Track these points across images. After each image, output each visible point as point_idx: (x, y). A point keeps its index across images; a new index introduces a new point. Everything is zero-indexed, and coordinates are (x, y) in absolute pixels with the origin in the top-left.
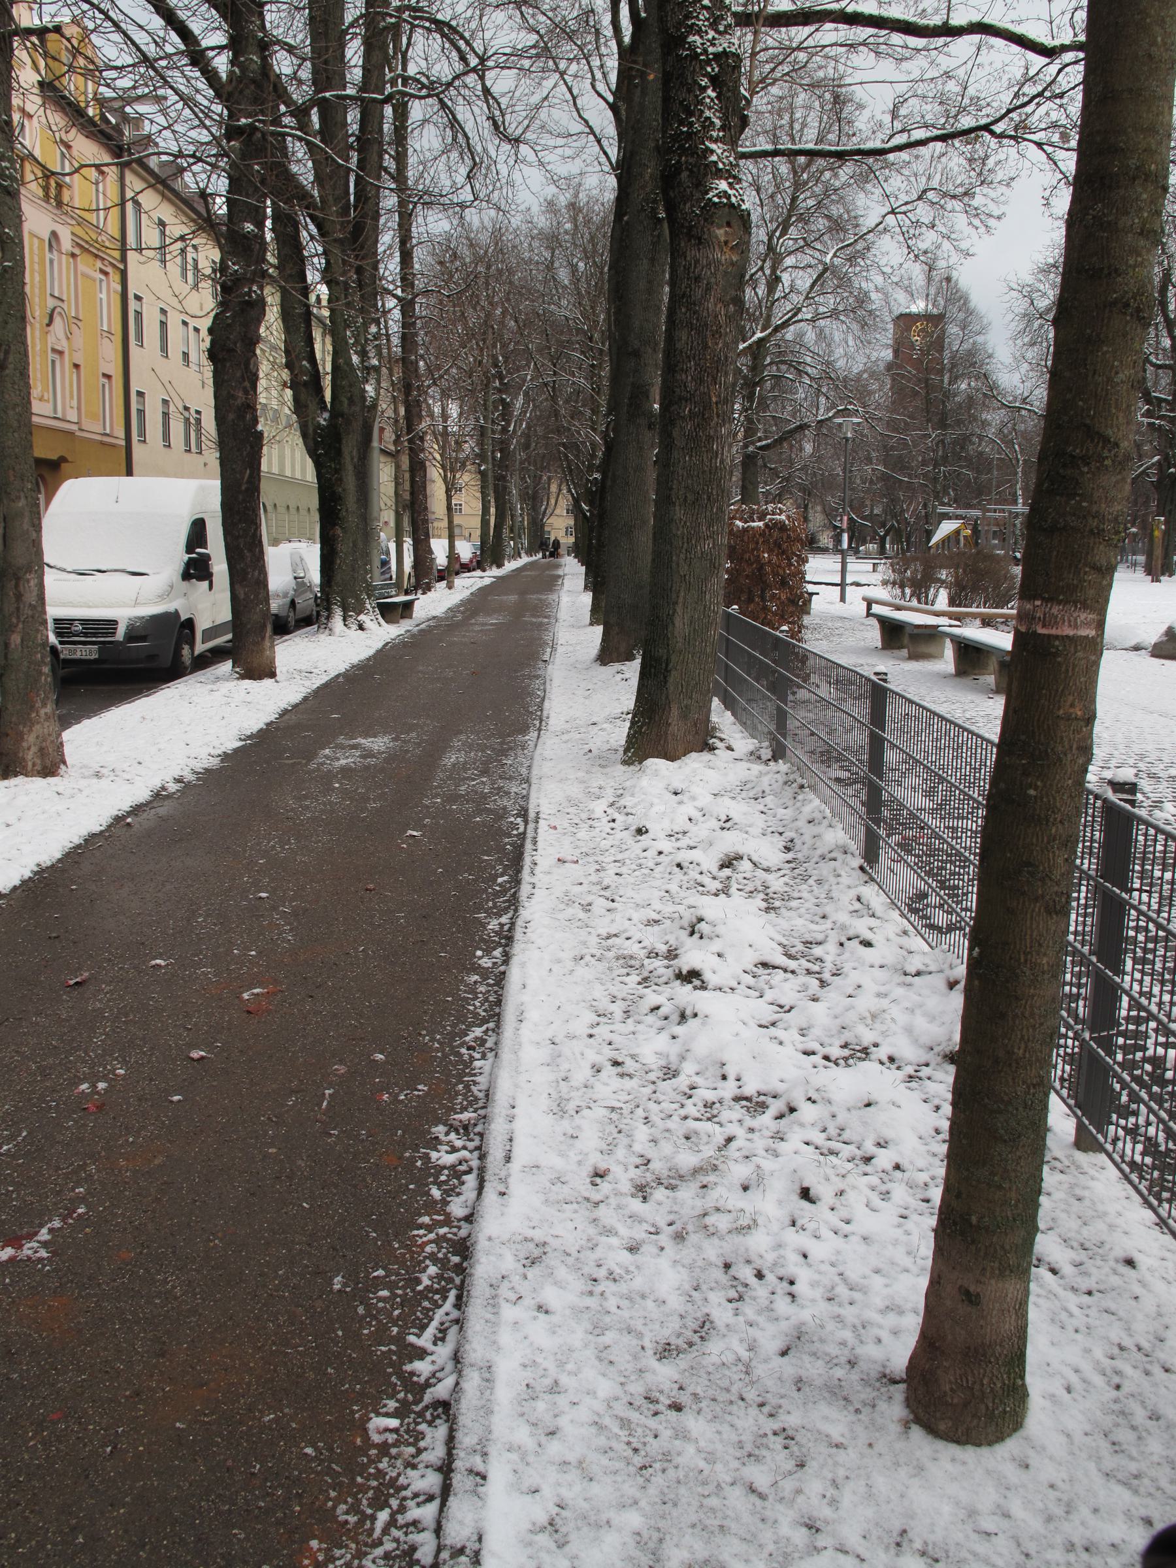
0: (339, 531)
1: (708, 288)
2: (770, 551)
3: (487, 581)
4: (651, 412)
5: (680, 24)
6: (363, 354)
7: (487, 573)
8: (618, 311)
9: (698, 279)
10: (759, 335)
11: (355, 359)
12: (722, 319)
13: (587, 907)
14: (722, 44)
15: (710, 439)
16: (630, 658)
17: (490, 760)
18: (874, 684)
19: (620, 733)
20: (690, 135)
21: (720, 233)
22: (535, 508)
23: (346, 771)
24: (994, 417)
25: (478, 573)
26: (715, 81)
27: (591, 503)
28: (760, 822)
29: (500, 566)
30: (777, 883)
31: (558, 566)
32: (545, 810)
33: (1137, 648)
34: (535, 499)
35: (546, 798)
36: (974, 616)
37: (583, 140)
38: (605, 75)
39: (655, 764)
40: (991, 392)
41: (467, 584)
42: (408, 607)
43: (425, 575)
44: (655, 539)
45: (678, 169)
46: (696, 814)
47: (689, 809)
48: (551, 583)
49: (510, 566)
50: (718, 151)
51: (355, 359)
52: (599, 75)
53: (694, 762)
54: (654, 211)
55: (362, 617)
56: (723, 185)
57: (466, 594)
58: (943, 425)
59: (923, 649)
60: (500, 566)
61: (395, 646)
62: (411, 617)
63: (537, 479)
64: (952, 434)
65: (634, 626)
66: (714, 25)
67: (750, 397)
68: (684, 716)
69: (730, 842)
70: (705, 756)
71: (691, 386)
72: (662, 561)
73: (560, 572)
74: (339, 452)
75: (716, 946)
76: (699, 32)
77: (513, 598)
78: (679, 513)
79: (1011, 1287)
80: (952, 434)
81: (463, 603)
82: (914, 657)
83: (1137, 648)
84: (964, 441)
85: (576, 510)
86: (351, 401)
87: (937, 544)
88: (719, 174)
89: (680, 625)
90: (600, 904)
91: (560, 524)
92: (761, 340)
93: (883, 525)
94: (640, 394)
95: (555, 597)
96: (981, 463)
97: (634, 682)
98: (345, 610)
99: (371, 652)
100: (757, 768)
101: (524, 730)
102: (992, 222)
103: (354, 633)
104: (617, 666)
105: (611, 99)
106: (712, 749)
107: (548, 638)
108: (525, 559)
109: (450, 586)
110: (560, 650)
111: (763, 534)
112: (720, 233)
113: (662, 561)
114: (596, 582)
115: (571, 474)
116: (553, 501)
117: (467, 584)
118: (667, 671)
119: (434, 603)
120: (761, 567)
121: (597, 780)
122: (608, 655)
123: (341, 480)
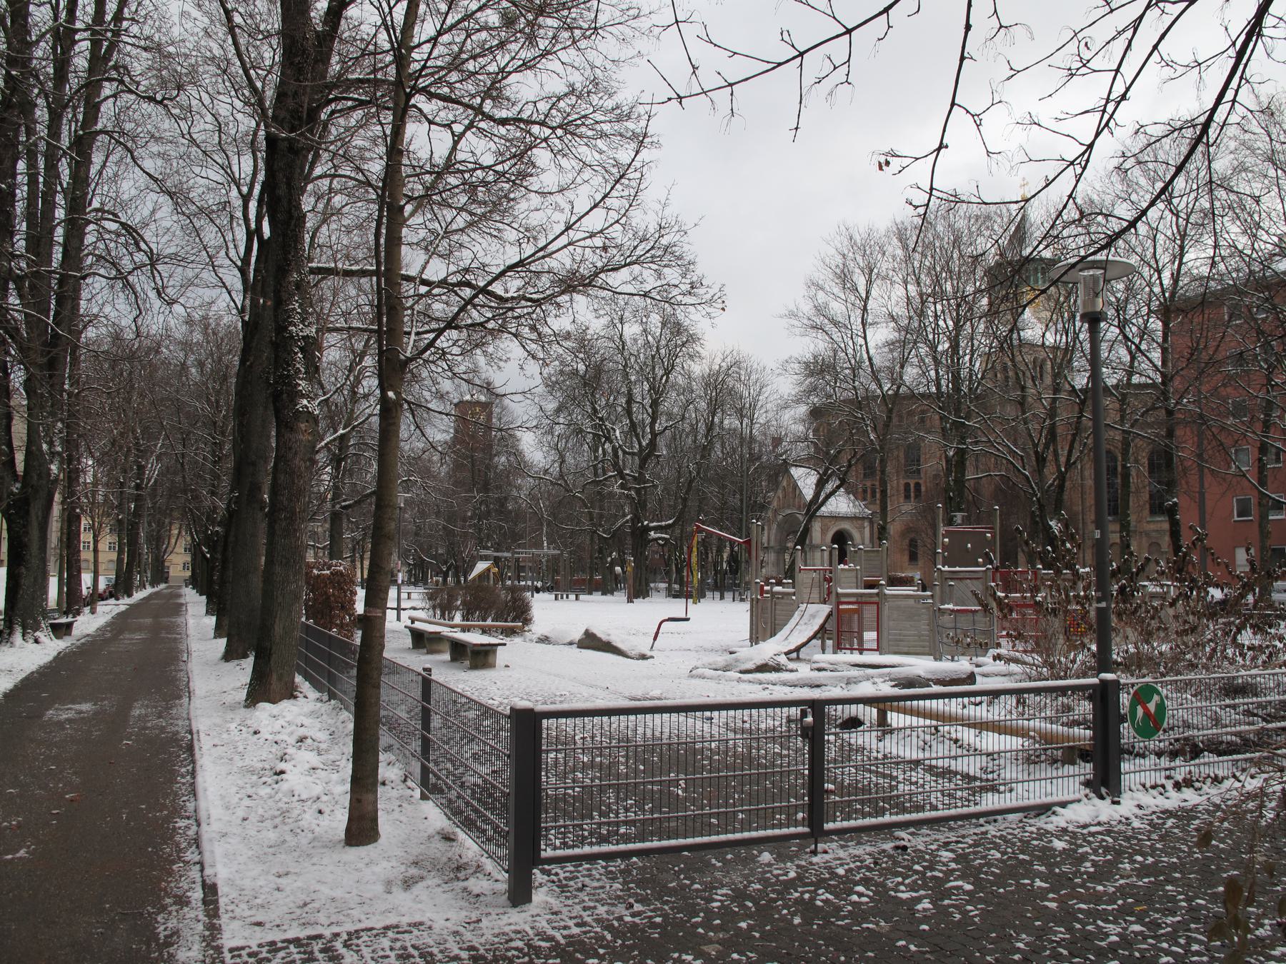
0: (23, 570)
1: (296, 453)
2: (334, 588)
3: (123, 608)
4: (263, 501)
5: (285, 320)
6: (51, 444)
7: (120, 602)
8: (241, 425)
9: (290, 448)
10: (341, 432)
11: (45, 447)
12: (303, 469)
13: (231, 760)
14: (307, 332)
15: (295, 530)
16: (245, 656)
17: (161, 712)
18: (424, 678)
19: (243, 695)
20: (288, 376)
21: (303, 426)
22: (158, 548)
23: (69, 721)
24: (526, 483)
25: (112, 601)
26: (302, 350)
27: (212, 549)
28: (319, 725)
29: (130, 595)
30: (323, 746)
31: (180, 596)
32: (202, 728)
33: (571, 643)
34: (158, 541)
35: (201, 724)
36: (474, 626)
37: (218, 290)
38: (235, 246)
39: (262, 705)
40: (520, 466)
41: (108, 611)
42: (69, 626)
43: (73, 601)
44: (264, 582)
45: (282, 393)
46: (285, 724)
47: (281, 722)
48: (177, 609)
49: (138, 596)
50: (303, 385)
51: (45, 447)
52: (231, 245)
53: (285, 705)
54: (268, 379)
55: (38, 634)
56: (305, 402)
57: (108, 618)
58: (485, 488)
59: (435, 647)
60: (130, 595)
61: (66, 654)
62: (70, 634)
63: (161, 525)
64: (494, 495)
65: (247, 634)
66: (303, 322)
67: (337, 468)
68: (280, 679)
69: (302, 732)
70: (292, 701)
71: (286, 503)
72: (268, 594)
73: (182, 600)
74: (27, 512)
75: (293, 762)
76: (295, 325)
77: (148, 621)
78: (278, 569)
79: (370, 797)
80: (494, 495)
81: (108, 624)
82: (430, 652)
83: (571, 643)
84: (502, 502)
85: (194, 550)
86: (40, 476)
87: (474, 579)
88: (303, 396)
89: (278, 629)
90: (237, 758)
91: (178, 561)
92: (342, 435)
93: (445, 563)
94: (255, 489)
95: (182, 619)
96: (518, 516)
97: (249, 670)
98: (24, 628)
99: (50, 658)
100: (319, 705)
101: (180, 697)
102: (501, 364)
103: (31, 645)
104: (236, 662)
105: (239, 263)
106: (296, 697)
107: (183, 647)
108: (149, 590)
109: (93, 612)
110: (194, 654)
111: (329, 578)
112: (303, 426)
113: (268, 594)
114: (217, 606)
115: (194, 521)
116: (173, 541)
117: (108, 611)
118: (270, 654)
119: (87, 624)
120: (328, 598)
121: (230, 715)
122: (229, 656)
123: (27, 533)
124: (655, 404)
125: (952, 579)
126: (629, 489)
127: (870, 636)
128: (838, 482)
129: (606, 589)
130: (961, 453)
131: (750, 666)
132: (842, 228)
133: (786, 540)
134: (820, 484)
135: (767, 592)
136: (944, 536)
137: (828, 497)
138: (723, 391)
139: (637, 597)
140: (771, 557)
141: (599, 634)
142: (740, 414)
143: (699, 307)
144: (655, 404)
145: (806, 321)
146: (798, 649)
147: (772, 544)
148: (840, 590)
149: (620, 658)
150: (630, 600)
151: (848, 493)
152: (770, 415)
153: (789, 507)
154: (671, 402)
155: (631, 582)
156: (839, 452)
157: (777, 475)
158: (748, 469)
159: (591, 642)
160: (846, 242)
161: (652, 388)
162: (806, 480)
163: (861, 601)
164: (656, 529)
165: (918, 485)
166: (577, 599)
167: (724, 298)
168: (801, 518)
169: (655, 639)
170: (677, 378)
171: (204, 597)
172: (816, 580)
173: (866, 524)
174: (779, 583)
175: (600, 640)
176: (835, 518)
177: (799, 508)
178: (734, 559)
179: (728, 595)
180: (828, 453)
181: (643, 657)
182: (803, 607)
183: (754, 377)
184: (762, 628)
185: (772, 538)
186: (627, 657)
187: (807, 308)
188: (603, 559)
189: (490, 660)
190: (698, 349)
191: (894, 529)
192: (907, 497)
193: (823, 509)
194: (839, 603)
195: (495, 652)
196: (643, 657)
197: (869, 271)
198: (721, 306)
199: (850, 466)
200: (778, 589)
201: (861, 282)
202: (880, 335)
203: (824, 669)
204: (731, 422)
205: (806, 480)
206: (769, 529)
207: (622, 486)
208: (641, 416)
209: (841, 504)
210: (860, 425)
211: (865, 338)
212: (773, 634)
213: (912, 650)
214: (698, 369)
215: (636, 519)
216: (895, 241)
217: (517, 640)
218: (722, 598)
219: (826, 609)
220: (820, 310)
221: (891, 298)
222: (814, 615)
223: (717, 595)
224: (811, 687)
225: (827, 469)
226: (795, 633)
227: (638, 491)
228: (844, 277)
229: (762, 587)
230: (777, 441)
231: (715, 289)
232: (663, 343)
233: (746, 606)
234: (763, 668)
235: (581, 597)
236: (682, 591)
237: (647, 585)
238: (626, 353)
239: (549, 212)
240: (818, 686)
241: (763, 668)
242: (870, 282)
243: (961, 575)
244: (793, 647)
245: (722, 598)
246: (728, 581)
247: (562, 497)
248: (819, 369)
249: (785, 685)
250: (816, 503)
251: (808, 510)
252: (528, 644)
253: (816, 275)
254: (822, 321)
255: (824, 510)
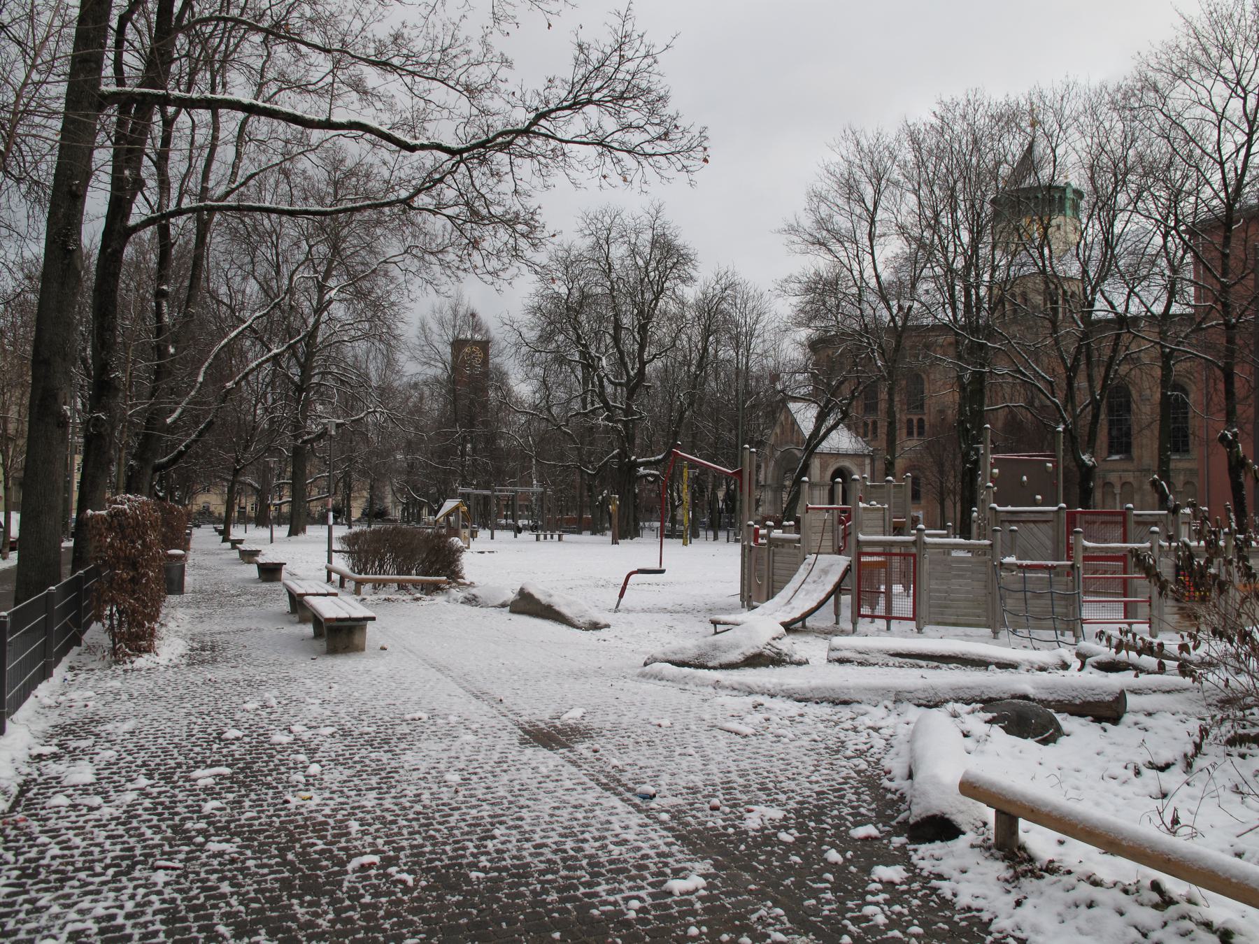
33: (503, 605)
40: (508, 401)
83: (503, 605)
84: (491, 439)
92: (276, 355)
124: (643, 329)
125: (1011, 522)
126: (616, 422)
127: (903, 604)
128: (840, 416)
129: (596, 529)
130: (979, 378)
131: (735, 656)
132: (849, 132)
133: (784, 479)
134: (821, 418)
135: (763, 537)
136: (993, 466)
137: (829, 431)
138: (716, 317)
139: (624, 537)
140: (768, 496)
141: (538, 595)
142: (736, 342)
143: (673, 158)
144: (643, 329)
145: (806, 237)
146: (803, 617)
147: (769, 482)
148: (861, 537)
149: (563, 629)
150: (615, 542)
151: (849, 429)
152: (768, 345)
153: (787, 443)
154: (661, 332)
155: (615, 521)
156: (842, 383)
157: (774, 412)
158: (744, 402)
159: (527, 605)
160: (852, 148)
161: (641, 312)
162: (805, 416)
163: (887, 550)
164: (647, 465)
165: (921, 421)
166: (560, 539)
167: (705, 144)
168: (799, 454)
169: (621, 595)
170: (667, 304)
171: (308, 528)
172: (829, 523)
173: (868, 461)
174: (778, 525)
175: (538, 602)
176: (838, 455)
177: (798, 444)
178: (731, 497)
179: (722, 535)
180: (829, 384)
181: (595, 626)
182: (811, 558)
183: (750, 305)
184: (759, 583)
185: (770, 475)
186: (577, 627)
187: (807, 222)
188: (592, 497)
189: (357, 639)
190: (690, 271)
191: (900, 463)
192: (910, 433)
193: (824, 443)
194: (860, 554)
195: (363, 628)
196: (595, 626)
197: (878, 177)
198: (701, 155)
199: (853, 397)
200: (777, 533)
201: (869, 193)
202: (892, 248)
203: (848, 661)
204: (726, 353)
205: (805, 416)
206: (767, 467)
207: (608, 418)
208: (630, 345)
209: (841, 440)
210: (863, 359)
211: (872, 254)
212: (771, 595)
213: (962, 619)
214: (691, 293)
215: (624, 454)
216: (906, 144)
217: (440, 599)
218: (716, 538)
219: (842, 562)
220: (822, 223)
221: (903, 207)
222: (820, 573)
223: (711, 534)
224: (836, 702)
225: (829, 401)
226: (801, 594)
227: (625, 424)
228: (850, 188)
229: (757, 530)
230: (775, 377)
231: (695, 131)
232: (653, 264)
233: (737, 548)
234: (755, 660)
235: (565, 537)
236: (670, 533)
237: (637, 524)
238: (613, 275)
239: (495, 67)
240: (846, 703)
241: (755, 660)
242: (878, 192)
243: (1024, 517)
244: (797, 614)
245: (716, 538)
246: (724, 520)
247: (552, 436)
248: (822, 292)
249: (789, 697)
250: (817, 437)
251: (808, 445)
252: (451, 606)
253: (819, 184)
254: (824, 236)
255: (825, 446)
